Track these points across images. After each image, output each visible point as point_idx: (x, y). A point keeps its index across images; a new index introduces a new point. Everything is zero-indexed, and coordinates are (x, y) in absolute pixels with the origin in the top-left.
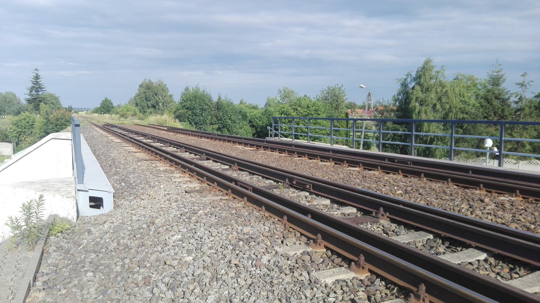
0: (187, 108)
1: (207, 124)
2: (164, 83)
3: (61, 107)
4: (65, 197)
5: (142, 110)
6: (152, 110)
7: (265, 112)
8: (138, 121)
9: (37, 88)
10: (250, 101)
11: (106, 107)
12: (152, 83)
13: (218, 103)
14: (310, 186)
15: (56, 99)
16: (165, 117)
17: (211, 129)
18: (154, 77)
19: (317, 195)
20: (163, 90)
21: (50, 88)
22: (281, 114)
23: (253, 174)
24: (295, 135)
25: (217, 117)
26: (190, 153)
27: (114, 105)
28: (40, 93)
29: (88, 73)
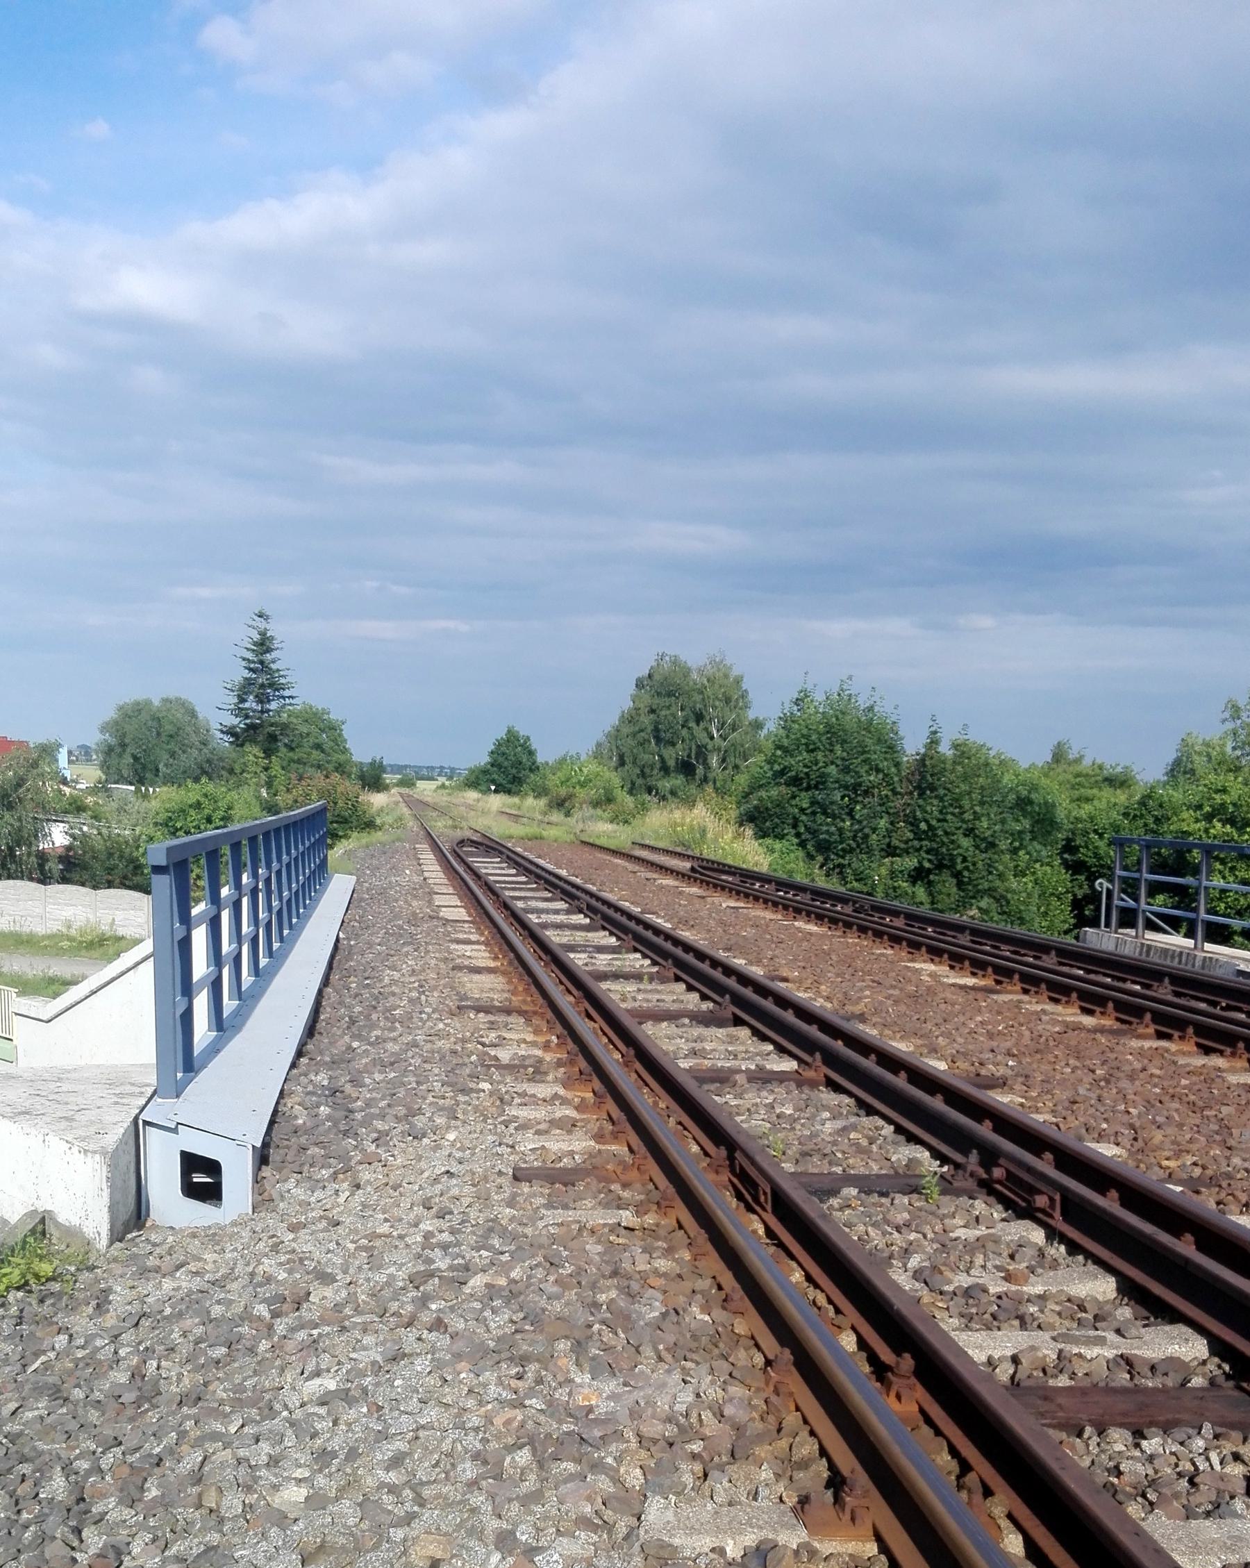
0: (795, 781)
1: (869, 852)
2: (735, 672)
3: (349, 761)
4: (75, 1149)
5: (639, 781)
6: (678, 781)
7: (1143, 803)
8: (609, 827)
9: (262, 686)
10: (1100, 750)
11: (510, 769)
12: (686, 672)
13: (922, 762)
14: (1052, 1200)
15: (333, 729)
16: (700, 814)
17: (884, 871)
18: (696, 646)
19: (1074, 1249)
20: (728, 700)
21: (307, 688)
22: (1209, 818)
23: (871, 1111)
24: (1209, 926)
25: (913, 823)
26: (690, 988)
27: (540, 759)
28: (273, 706)
29: (464, 627)
